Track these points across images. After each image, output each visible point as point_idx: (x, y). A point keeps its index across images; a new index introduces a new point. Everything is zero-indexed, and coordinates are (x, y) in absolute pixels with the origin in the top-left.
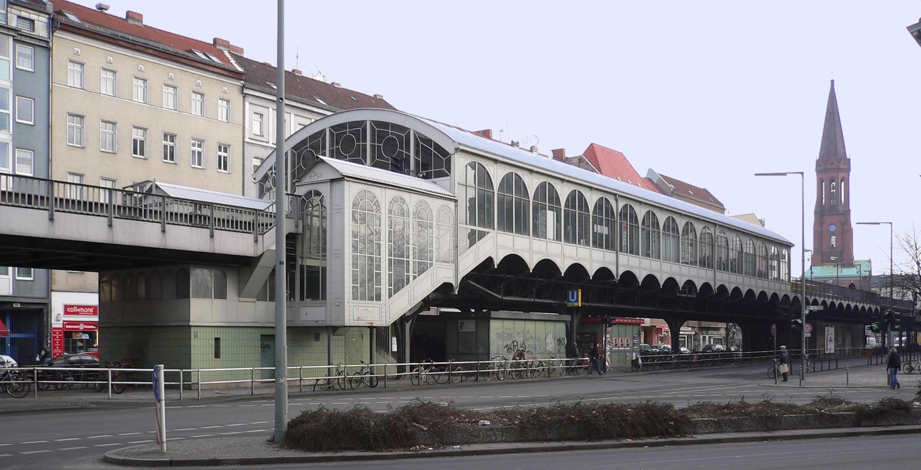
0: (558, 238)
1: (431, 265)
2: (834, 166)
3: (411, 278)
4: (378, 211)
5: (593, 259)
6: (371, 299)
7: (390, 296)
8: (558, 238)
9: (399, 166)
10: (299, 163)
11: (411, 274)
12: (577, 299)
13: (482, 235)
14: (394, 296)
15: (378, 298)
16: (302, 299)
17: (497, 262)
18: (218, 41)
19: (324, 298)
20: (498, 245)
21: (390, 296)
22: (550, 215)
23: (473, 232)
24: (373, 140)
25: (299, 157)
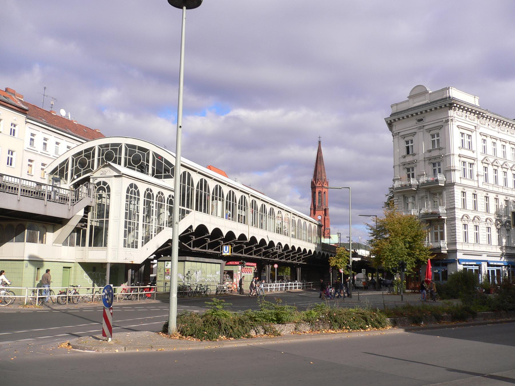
0: (222, 217)
1: (163, 228)
2: (320, 185)
3: (153, 236)
4: (139, 195)
5: (238, 229)
6: (133, 247)
7: (142, 246)
8: (222, 217)
9: (143, 169)
10: (76, 165)
11: (153, 233)
12: (227, 251)
13: (188, 212)
14: (144, 246)
15: (137, 247)
16: (90, 245)
17: (194, 228)
18: (9, 90)
19: (105, 245)
20: (195, 219)
21: (142, 246)
22: (220, 203)
23: (183, 210)
24: (126, 154)
25: (76, 162)
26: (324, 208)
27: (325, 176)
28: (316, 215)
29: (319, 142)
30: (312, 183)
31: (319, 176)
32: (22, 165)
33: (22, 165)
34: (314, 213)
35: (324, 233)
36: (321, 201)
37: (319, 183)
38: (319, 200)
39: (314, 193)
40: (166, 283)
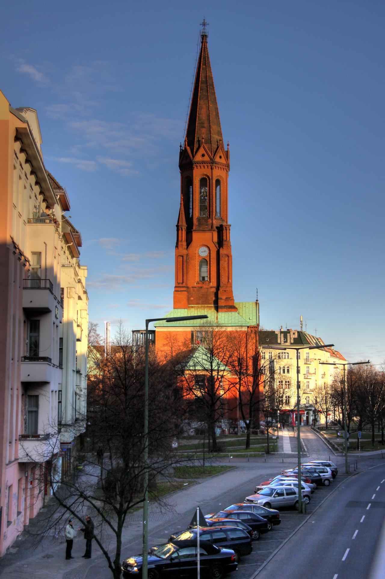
2: (206, 158)
26: (216, 223)
27: (220, 133)
28: (193, 244)
29: (204, 37)
30: (183, 154)
31: (201, 133)
32: (61, 349)
33: (61, 349)
34: (189, 241)
35: (216, 294)
36: (207, 207)
37: (201, 151)
38: (202, 201)
39: (187, 183)
40: (63, 266)
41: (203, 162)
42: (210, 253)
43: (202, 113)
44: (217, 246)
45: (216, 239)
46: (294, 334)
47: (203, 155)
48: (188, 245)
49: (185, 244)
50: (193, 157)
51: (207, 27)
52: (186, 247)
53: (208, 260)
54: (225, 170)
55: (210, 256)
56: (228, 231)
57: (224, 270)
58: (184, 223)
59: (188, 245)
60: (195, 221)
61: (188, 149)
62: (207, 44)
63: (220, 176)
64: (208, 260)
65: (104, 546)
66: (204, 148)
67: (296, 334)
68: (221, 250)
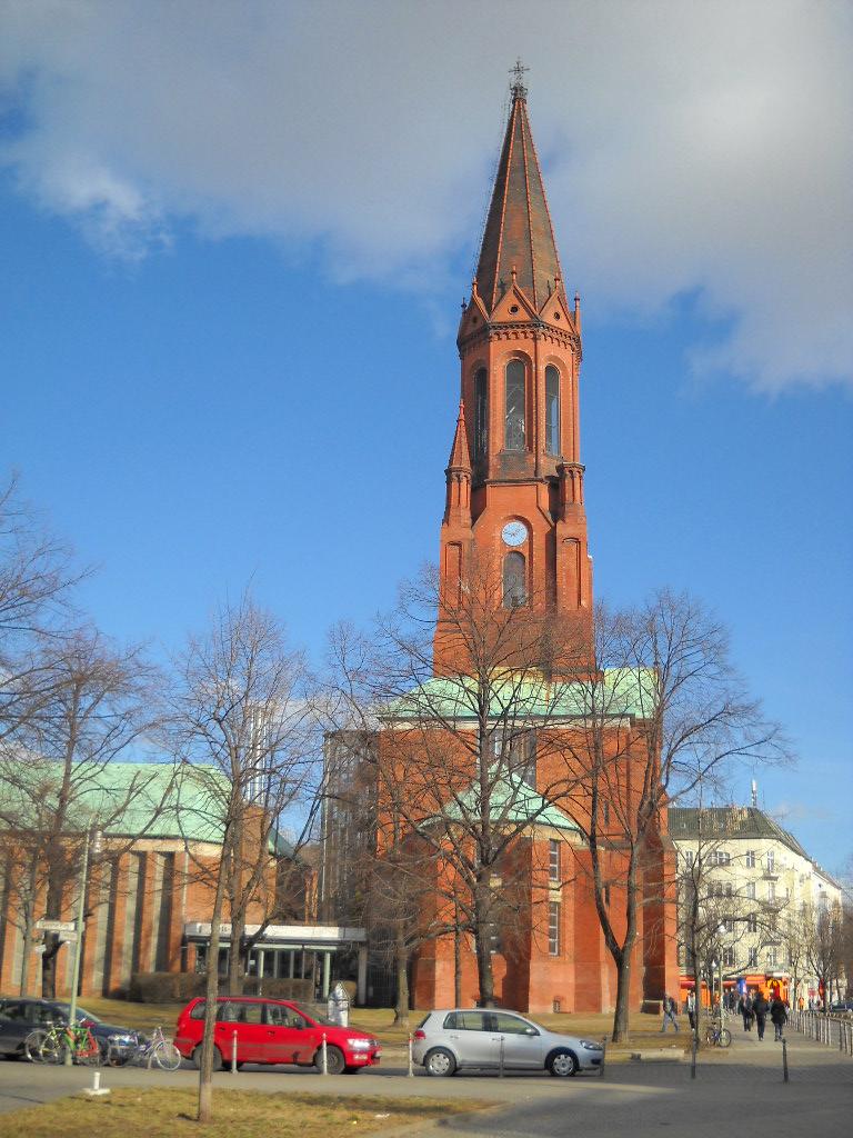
2: (522, 315)
26: (548, 467)
39: (476, 383)
41: (512, 325)
42: (531, 537)
43: (510, 225)
44: (549, 515)
45: (545, 503)
46: (741, 812)
47: (514, 309)
48: (476, 513)
49: (466, 515)
50: (489, 310)
51: (525, 75)
52: (469, 522)
53: (527, 555)
54: (569, 347)
55: (531, 544)
56: (577, 480)
57: (568, 576)
58: (466, 465)
59: (474, 518)
60: (493, 460)
61: (480, 301)
62: (527, 107)
63: (556, 359)
64: (527, 555)
65: (27, 967)
66: (516, 292)
67: (746, 814)
68: (560, 525)
